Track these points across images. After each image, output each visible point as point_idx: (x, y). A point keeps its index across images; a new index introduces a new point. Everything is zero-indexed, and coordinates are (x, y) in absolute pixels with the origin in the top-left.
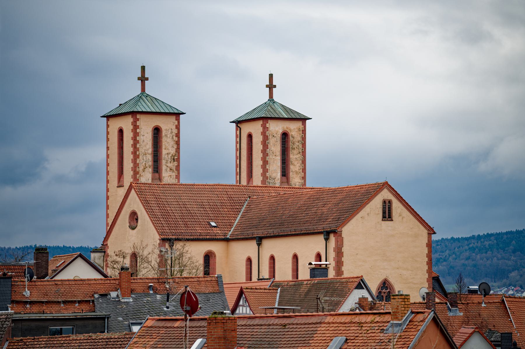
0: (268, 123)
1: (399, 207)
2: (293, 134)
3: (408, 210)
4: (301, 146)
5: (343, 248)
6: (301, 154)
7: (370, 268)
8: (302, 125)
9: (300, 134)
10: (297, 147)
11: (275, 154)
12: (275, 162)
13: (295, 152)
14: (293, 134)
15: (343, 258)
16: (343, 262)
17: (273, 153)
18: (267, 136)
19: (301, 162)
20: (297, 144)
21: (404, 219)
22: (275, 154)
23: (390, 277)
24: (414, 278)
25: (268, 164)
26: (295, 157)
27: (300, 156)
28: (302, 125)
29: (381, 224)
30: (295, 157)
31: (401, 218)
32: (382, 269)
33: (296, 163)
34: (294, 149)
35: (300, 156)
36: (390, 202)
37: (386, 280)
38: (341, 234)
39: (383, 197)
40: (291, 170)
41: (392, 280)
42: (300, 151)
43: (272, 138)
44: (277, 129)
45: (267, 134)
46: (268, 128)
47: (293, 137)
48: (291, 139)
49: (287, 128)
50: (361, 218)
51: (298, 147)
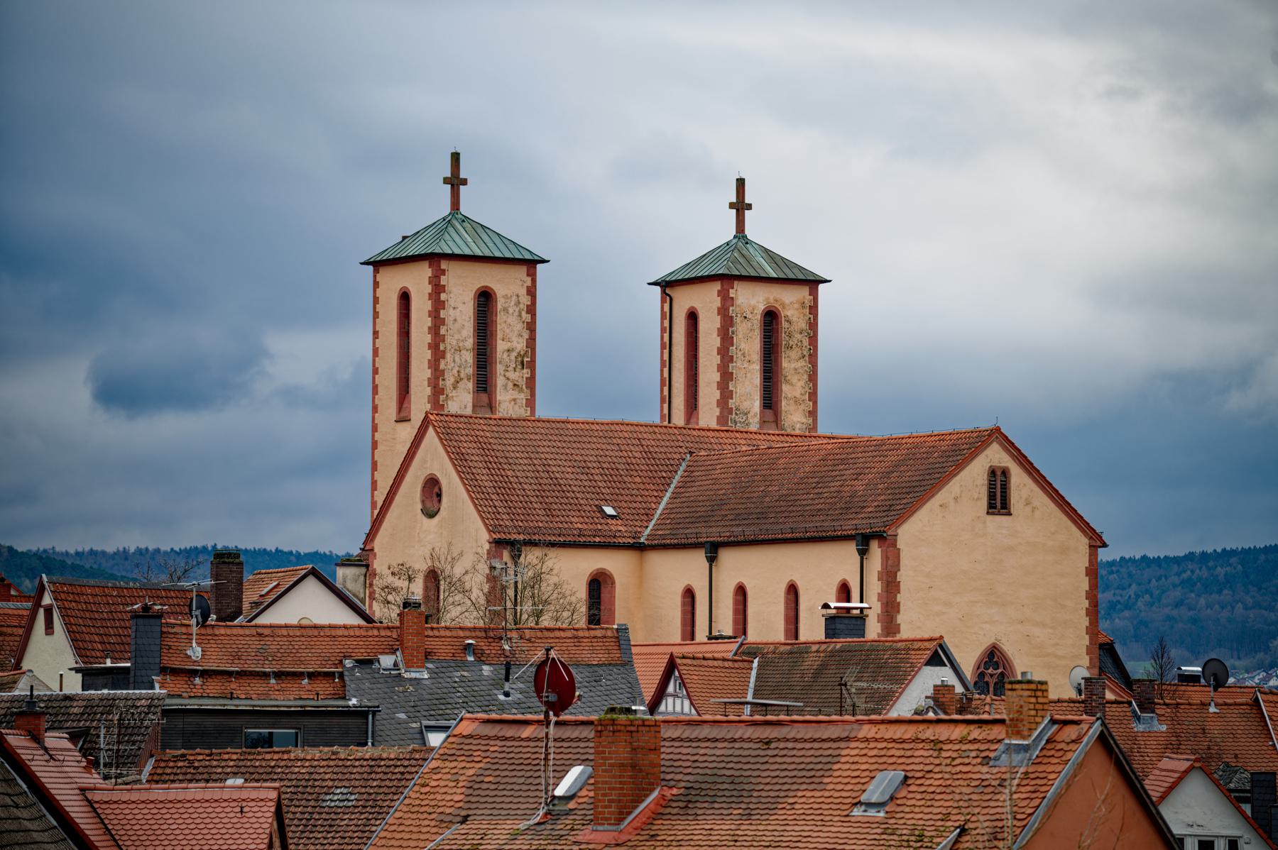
0: (733, 288)
1: (1025, 485)
2: (789, 313)
3: (1045, 493)
4: (806, 342)
5: (899, 574)
6: (807, 358)
7: (960, 619)
8: (810, 295)
9: (804, 315)
10: (797, 345)
11: (747, 358)
12: (749, 375)
13: (794, 354)
14: (789, 314)
15: (898, 595)
16: (899, 603)
17: (744, 355)
18: (732, 317)
19: (806, 377)
20: (798, 336)
21: (1037, 513)
22: (747, 358)
23: (1004, 640)
24: (1057, 644)
25: (732, 380)
26: (793, 366)
27: (804, 364)
28: (810, 295)
29: (984, 522)
30: (793, 366)
31: (1028, 509)
32: (986, 622)
33: (794, 379)
34: (791, 347)
35: (804, 364)
36: (1005, 473)
37: (994, 647)
38: (896, 541)
39: (989, 460)
40: (783, 395)
41: (1008, 648)
42: (805, 353)
43: (742, 322)
44: (753, 302)
45: (731, 312)
46: (732, 298)
47: (789, 322)
48: (785, 325)
49: (776, 301)
50: (941, 506)
51: (799, 344)
